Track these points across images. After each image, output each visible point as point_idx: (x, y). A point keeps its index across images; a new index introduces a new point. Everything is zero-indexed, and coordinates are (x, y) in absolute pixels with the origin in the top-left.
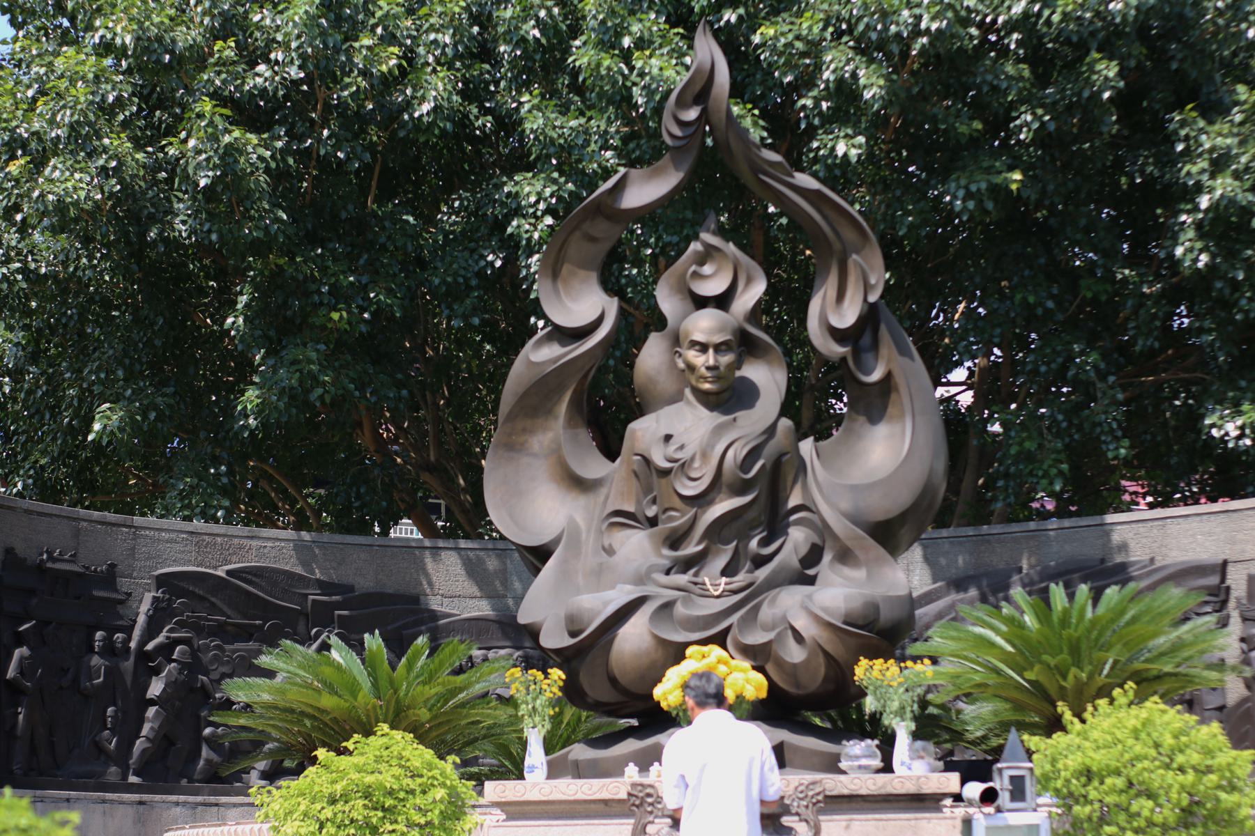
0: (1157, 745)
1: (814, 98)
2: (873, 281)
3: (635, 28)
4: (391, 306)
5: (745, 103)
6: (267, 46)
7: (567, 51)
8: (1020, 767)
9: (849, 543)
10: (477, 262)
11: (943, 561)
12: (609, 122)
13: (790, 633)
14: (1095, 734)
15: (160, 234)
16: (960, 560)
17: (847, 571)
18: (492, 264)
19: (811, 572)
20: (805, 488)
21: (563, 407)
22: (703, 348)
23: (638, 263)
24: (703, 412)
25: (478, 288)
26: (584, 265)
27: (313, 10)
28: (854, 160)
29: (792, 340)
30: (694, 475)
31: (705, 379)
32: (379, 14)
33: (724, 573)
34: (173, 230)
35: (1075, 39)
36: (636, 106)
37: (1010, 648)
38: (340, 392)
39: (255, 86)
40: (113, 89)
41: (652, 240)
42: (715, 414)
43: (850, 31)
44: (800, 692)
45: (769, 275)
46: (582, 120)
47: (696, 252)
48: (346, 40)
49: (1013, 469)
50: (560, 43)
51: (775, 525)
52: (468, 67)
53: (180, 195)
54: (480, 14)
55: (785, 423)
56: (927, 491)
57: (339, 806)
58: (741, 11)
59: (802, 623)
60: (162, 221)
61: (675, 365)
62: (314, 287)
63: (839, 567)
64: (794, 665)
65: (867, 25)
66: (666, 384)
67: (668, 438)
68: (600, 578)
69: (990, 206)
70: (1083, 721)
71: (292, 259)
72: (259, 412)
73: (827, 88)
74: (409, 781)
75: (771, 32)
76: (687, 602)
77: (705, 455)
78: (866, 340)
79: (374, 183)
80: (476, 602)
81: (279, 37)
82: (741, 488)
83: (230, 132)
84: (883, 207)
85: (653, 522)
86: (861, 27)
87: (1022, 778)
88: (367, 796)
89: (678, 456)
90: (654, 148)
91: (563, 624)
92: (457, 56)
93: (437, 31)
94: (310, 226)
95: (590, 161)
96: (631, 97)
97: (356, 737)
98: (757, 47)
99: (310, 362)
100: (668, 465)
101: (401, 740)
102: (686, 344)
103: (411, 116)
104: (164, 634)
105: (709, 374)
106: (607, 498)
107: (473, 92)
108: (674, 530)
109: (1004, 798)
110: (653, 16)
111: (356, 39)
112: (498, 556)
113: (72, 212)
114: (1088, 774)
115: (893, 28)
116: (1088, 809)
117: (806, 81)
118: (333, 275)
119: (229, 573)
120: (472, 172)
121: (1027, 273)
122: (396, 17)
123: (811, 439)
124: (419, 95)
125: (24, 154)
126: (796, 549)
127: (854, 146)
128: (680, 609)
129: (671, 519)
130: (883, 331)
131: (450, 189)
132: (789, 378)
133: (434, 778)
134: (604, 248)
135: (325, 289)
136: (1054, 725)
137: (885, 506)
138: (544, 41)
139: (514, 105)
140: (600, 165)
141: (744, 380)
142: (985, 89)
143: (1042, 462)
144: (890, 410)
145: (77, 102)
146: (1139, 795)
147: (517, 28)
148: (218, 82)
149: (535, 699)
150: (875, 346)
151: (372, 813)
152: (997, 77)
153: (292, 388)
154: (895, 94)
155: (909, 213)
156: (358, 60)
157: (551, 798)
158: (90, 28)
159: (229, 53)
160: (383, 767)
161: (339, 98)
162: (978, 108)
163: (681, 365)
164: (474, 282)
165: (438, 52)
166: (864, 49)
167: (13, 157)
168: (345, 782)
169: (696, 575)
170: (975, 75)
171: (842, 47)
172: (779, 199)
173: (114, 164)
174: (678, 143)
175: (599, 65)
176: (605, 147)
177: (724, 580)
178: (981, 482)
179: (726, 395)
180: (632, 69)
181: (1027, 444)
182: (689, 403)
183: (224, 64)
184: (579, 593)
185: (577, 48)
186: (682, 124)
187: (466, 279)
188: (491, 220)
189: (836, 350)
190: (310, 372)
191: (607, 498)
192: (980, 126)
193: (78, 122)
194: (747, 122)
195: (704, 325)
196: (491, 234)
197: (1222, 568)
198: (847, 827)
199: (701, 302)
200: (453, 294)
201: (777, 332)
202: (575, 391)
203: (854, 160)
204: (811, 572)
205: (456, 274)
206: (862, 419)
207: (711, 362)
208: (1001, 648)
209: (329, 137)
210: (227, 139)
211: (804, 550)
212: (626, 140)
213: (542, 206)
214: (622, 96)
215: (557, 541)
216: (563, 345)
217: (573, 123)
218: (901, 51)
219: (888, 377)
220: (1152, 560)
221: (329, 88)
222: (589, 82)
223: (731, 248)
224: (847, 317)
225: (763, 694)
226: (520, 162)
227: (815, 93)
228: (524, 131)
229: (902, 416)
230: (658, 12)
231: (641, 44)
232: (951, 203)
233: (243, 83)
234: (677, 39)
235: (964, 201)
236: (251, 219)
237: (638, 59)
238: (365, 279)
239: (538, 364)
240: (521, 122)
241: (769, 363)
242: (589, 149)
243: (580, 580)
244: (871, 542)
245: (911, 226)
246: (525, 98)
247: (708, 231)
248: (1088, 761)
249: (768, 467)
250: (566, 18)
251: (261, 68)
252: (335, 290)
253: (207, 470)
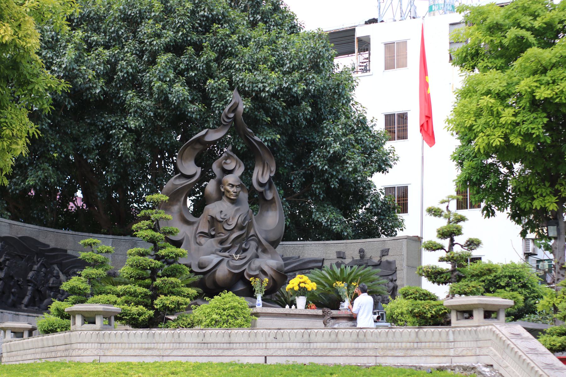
2: (272, 170)
22: (233, 186)
30: (229, 223)
59: (266, 269)
67: (221, 212)
104: (3, 257)
106: (198, 227)
108: (223, 239)
129: (221, 236)
197: (323, 261)
215: (183, 239)
223: (235, 156)
239: (176, 185)
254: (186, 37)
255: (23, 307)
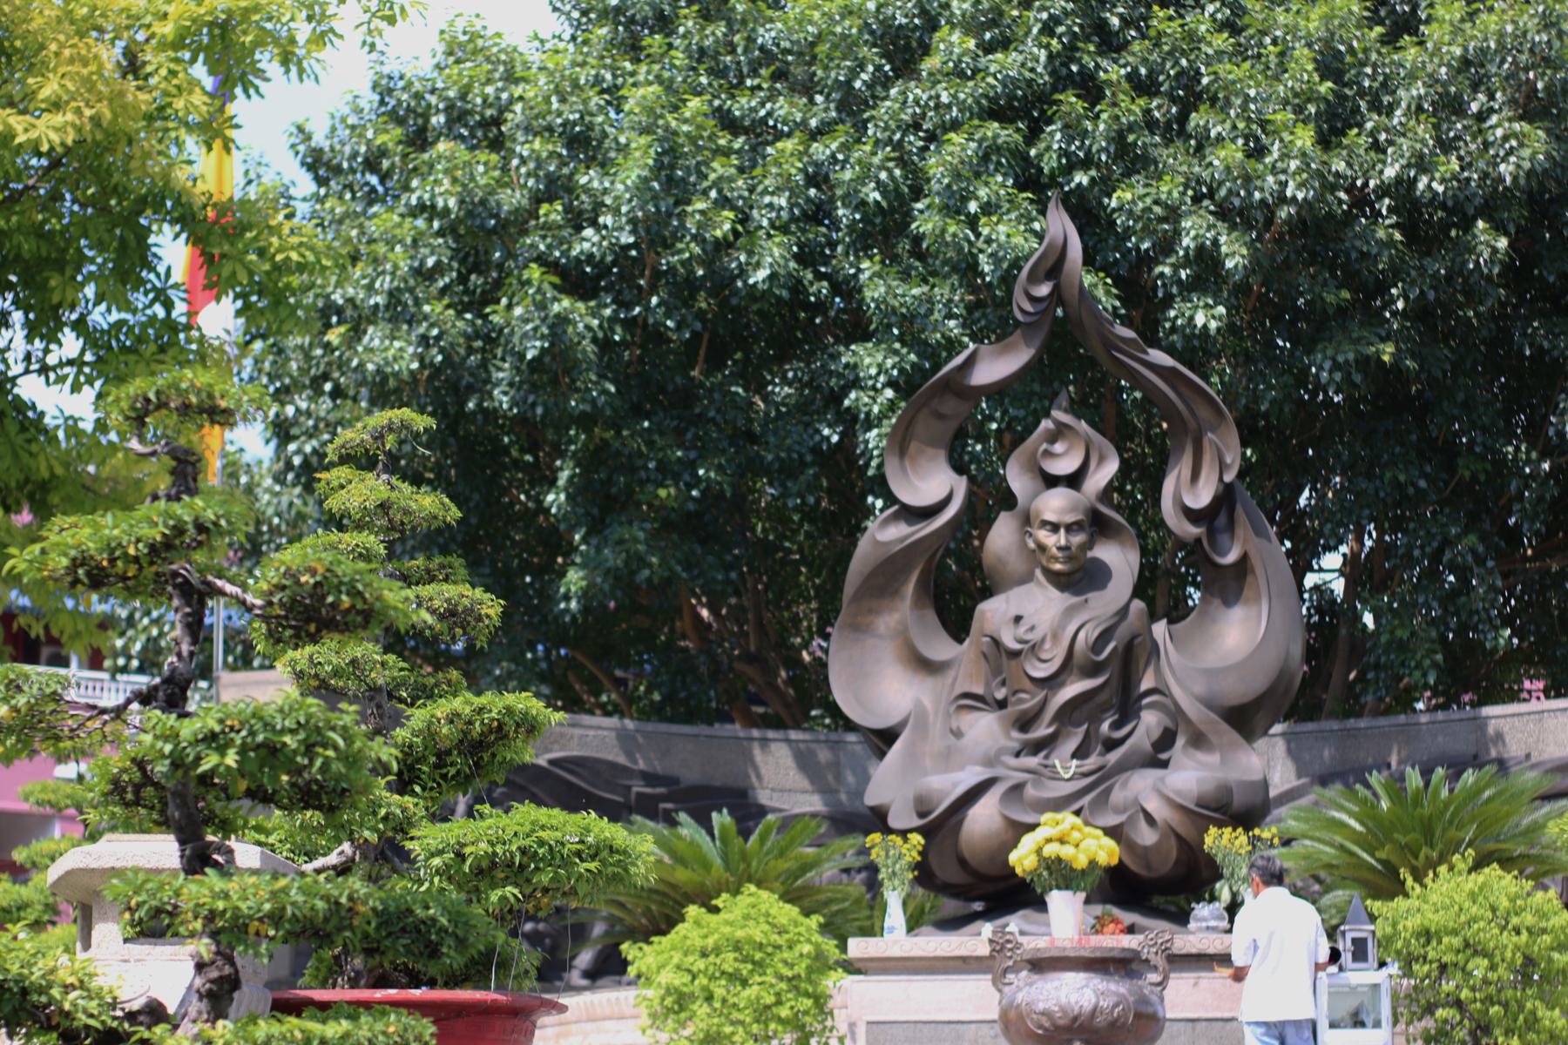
0: (1494, 909)
1: (1173, 265)
2: (1228, 460)
3: (983, 193)
4: (720, 483)
5: (1097, 271)
6: (594, 210)
7: (908, 217)
8: (1364, 930)
9: (1203, 728)
10: (812, 437)
11: (1307, 756)
12: (953, 290)
13: (1141, 816)
14: (1434, 898)
15: (479, 405)
16: (1326, 754)
17: (1200, 756)
18: (828, 438)
19: (1164, 756)
20: (1158, 672)
21: (910, 588)
22: (1055, 527)
23: (982, 437)
24: (1054, 593)
25: (813, 464)
26: (933, 443)
27: (645, 173)
28: (1213, 332)
29: (1145, 520)
30: (1044, 656)
31: (1056, 559)
32: (713, 176)
33: (1075, 755)
34: (492, 398)
35: (1450, 203)
36: (982, 275)
37: (1358, 827)
38: (666, 574)
39: (582, 252)
40: (432, 253)
41: (998, 414)
42: (1066, 595)
43: (1211, 195)
44: (1153, 875)
45: (1120, 450)
46: (926, 289)
47: (1047, 430)
48: (677, 203)
49: (1383, 659)
50: (901, 206)
51: (1127, 709)
52: (804, 231)
53: (499, 364)
54: (816, 174)
55: (1138, 605)
56: (1283, 676)
57: (712, 959)
58: (1093, 173)
59: (1154, 806)
60: (481, 391)
61: (1026, 545)
62: (639, 462)
63: (1191, 751)
64: (1146, 848)
65: (1230, 191)
66: (1016, 564)
67: (1018, 619)
68: (948, 760)
69: (1357, 378)
70: (1424, 886)
71: (618, 433)
72: (585, 595)
73: (1187, 254)
74: (776, 937)
75: (1128, 196)
76: (1037, 784)
77: (1055, 637)
78: (1222, 520)
79: (702, 353)
80: (807, 797)
81: (608, 201)
82: (1092, 670)
83: (559, 300)
84: (1244, 381)
85: (1002, 704)
86: (1223, 192)
87: (1364, 940)
88: (737, 947)
89: (1029, 637)
90: (1001, 318)
91: (911, 804)
92: (793, 219)
93: (772, 194)
94: (635, 399)
95: (935, 330)
96: (977, 264)
97: (724, 896)
98: (1114, 210)
99: (636, 540)
100: (1017, 646)
101: (767, 900)
102: (1037, 523)
103: (745, 282)
105: (1060, 554)
106: (955, 680)
107: (807, 256)
108: (1024, 712)
109: (1346, 958)
110: (1000, 178)
111: (689, 203)
112: (832, 748)
113: (392, 383)
114: (1427, 935)
115: (1257, 195)
116: (1426, 968)
117: (1166, 246)
118: (661, 449)
119: (551, 762)
120: (805, 341)
121: (1397, 450)
122: (731, 180)
123: (1164, 621)
124: (754, 261)
125: (339, 323)
126: (1148, 733)
127: (1213, 317)
128: (1030, 791)
129: (1022, 701)
130: (1239, 510)
131: (783, 358)
132: (1142, 564)
133: (799, 934)
134: (950, 427)
135: (651, 465)
136: (1399, 889)
137: (1240, 690)
138: (884, 204)
139: (852, 271)
140: (943, 336)
141: (1096, 561)
142: (1354, 255)
143: (1415, 652)
144: (1245, 592)
145: (396, 267)
146: (1476, 953)
147: (857, 191)
148: (542, 247)
149: (894, 864)
150: (1231, 526)
151: (742, 966)
152: (1368, 243)
153: (617, 569)
154: (1259, 264)
155: (1270, 387)
156: (691, 225)
157: (912, 954)
158: (407, 188)
159: (553, 216)
160: (752, 923)
161: (668, 263)
162: (1350, 279)
163: (1032, 545)
164: (809, 458)
165: (774, 215)
166: (1223, 213)
167: (328, 326)
168: (716, 936)
169: (1046, 757)
170: (1343, 241)
171: (1202, 212)
172: (1137, 381)
173: (435, 332)
174: (1029, 319)
175: (943, 231)
176: (950, 316)
177: (1075, 762)
178: (1352, 676)
179: (1078, 576)
180: (978, 235)
181: (1399, 633)
182: (1039, 583)
183: (550, 229)
184: (926, 774)
185: (921, 212)
186: (1033, 300)
187: (801, 456)
188: (826, 391)
189: (1191, 531)
190: (636, 552)
191: (955, 680)
192: (1348, 296)
193: (398, 289)
194: (1100, 293)
195: (1055, 505)
196: (826, 408)
198: (1196, 984)
199: (1051, 481)
200: (786, 472)
201: (1131, 512)
202: (922, 572)
203: (1213, 332)
204: (1164, 756)
205: (789, 450)
206: (1217, 602)
207: (1063, 542)
208: (1354, 830)
209: (659, 305)
210: (556, 308)
211: (1156, 734)
212: (970, 308)
213: (882, 379)
214: (968, 264)
215: (903, 724)
216: (910, 523)
217: (916, 291)
218: (1266, 217)
219: (1244, 558)
220: (1528, 756)
221: (658, 254)
222: (933, 249)
223: (1083, 426)
224: (1202, 497)
225: (1115, 861)
226: (857, 328)
227: (1172, 260)
228: (863, 299)
229: (1258, 599)
230: (1005, 175)
231: (988, 209)
232: (1317, 375)
233: (569, 249)
234: (1026, 204)
235: (1331, 372)
236: (577, 390)
237: (985, 225)
238: (693, 455)
240: (860, 291)
241: (1122, 543)
242: (932, 318)
243: (928, 762)
244: (1225, 726)
245: (1273, 402)
246: (865, 265)
247: (1059, 408)
248: (1426, 923)
249: (1120, 649)
250: (907, 178)
251: (589, 232)
252: (663, 467)
253: (524, 655)
254: (1066, 65)
255: (575, 977)
